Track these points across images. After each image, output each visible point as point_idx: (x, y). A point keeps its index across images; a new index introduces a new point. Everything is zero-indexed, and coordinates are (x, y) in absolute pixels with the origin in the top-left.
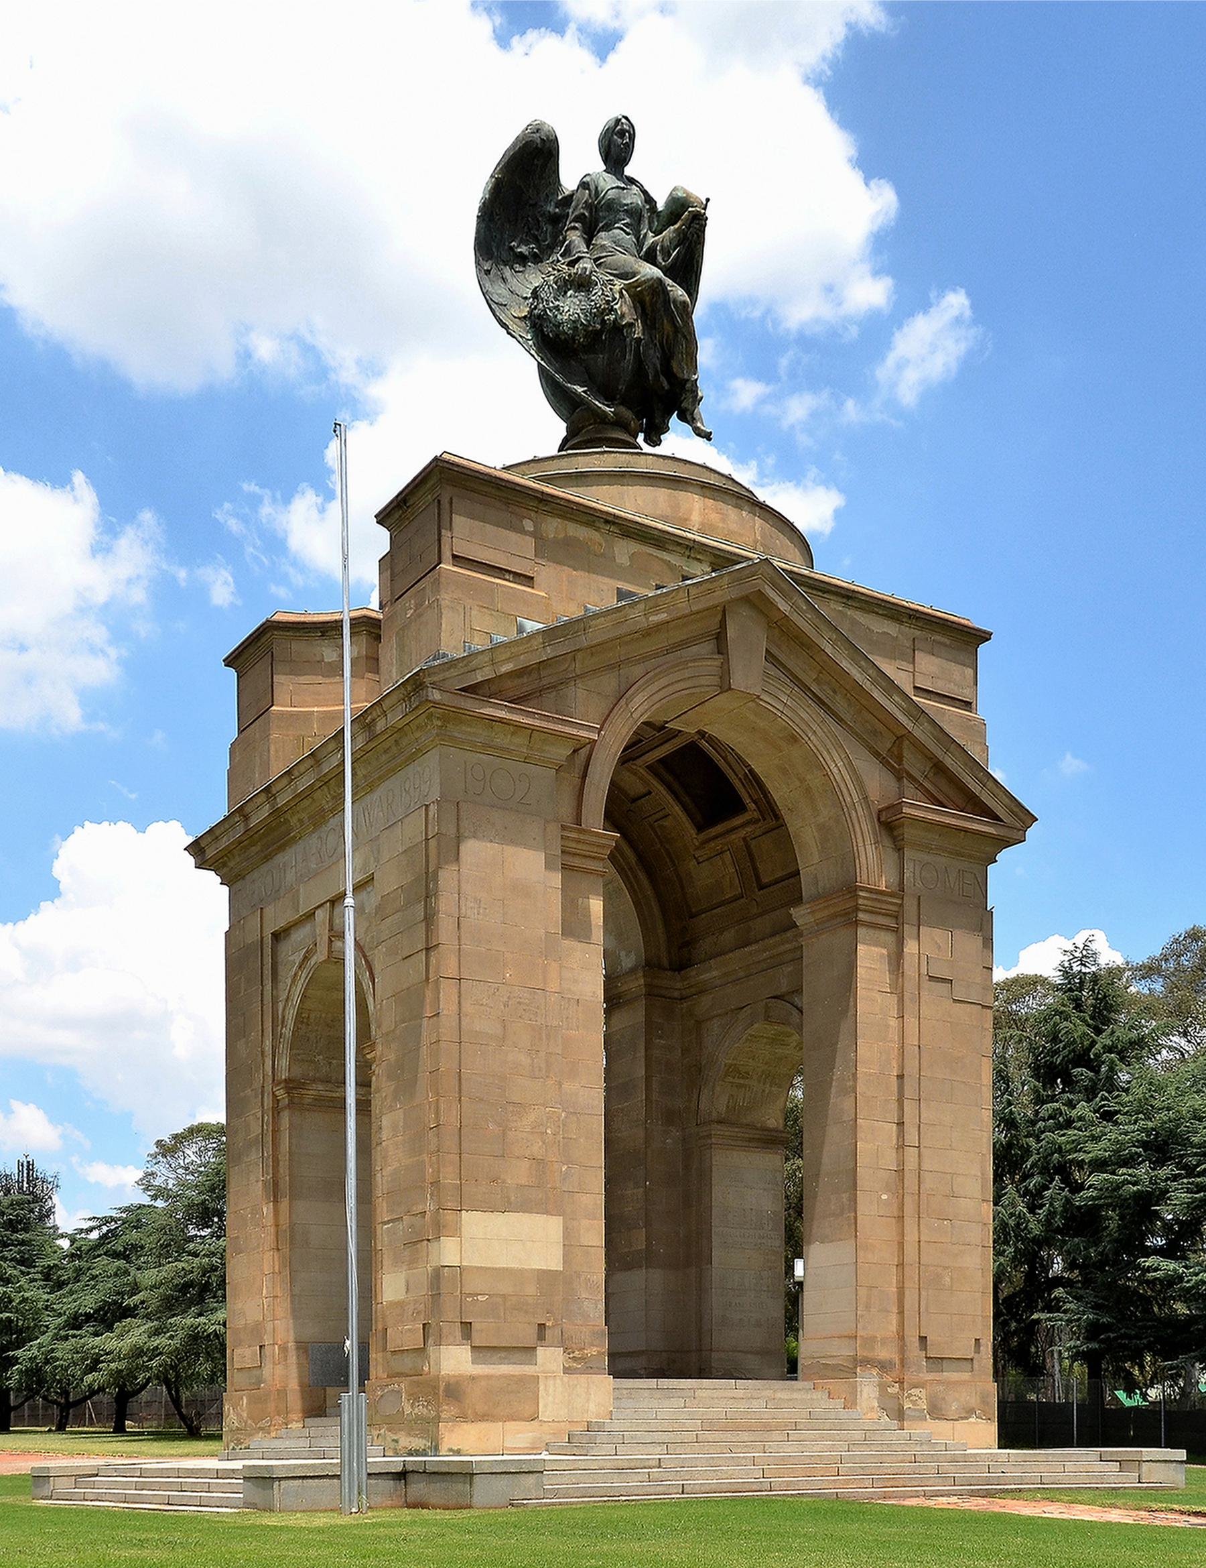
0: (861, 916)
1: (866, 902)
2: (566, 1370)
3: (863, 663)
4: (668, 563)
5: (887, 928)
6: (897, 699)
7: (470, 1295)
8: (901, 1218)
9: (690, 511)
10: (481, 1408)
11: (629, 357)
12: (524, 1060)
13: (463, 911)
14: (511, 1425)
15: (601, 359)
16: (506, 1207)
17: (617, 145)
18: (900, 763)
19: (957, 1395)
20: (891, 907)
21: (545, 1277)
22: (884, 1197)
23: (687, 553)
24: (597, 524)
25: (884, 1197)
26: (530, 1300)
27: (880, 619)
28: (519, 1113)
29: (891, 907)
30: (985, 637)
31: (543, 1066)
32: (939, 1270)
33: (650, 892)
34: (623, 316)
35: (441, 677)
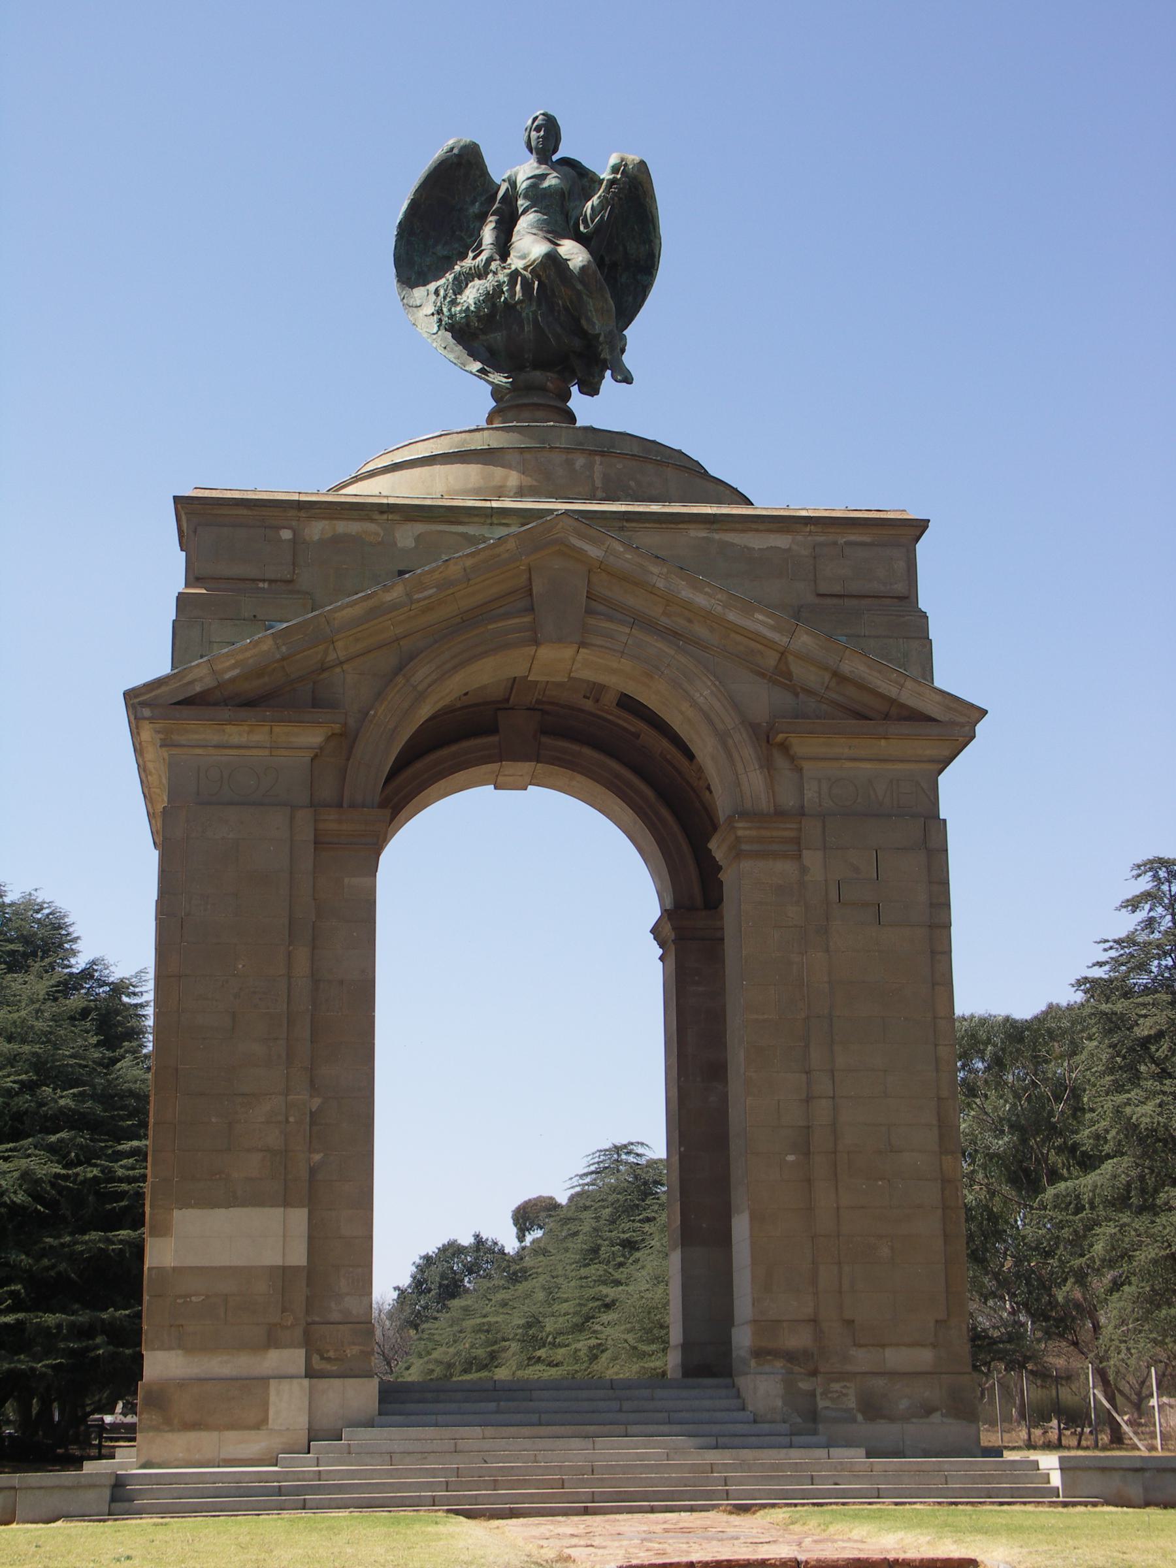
0: (744, 847)
1: (747, 833)
2: (310, 1374)
3: (707, 589)
6: (761, 617)
7: (179, 1297)
14: (231, 1435)
16: (232, 1200)
17: (547, 135)
18: (790, 679)
21: (285, 1273)
22: (791, 1158)
23: (489, 521)
25: (791, 1158)
30: (921, 526)
33: (676, 828)
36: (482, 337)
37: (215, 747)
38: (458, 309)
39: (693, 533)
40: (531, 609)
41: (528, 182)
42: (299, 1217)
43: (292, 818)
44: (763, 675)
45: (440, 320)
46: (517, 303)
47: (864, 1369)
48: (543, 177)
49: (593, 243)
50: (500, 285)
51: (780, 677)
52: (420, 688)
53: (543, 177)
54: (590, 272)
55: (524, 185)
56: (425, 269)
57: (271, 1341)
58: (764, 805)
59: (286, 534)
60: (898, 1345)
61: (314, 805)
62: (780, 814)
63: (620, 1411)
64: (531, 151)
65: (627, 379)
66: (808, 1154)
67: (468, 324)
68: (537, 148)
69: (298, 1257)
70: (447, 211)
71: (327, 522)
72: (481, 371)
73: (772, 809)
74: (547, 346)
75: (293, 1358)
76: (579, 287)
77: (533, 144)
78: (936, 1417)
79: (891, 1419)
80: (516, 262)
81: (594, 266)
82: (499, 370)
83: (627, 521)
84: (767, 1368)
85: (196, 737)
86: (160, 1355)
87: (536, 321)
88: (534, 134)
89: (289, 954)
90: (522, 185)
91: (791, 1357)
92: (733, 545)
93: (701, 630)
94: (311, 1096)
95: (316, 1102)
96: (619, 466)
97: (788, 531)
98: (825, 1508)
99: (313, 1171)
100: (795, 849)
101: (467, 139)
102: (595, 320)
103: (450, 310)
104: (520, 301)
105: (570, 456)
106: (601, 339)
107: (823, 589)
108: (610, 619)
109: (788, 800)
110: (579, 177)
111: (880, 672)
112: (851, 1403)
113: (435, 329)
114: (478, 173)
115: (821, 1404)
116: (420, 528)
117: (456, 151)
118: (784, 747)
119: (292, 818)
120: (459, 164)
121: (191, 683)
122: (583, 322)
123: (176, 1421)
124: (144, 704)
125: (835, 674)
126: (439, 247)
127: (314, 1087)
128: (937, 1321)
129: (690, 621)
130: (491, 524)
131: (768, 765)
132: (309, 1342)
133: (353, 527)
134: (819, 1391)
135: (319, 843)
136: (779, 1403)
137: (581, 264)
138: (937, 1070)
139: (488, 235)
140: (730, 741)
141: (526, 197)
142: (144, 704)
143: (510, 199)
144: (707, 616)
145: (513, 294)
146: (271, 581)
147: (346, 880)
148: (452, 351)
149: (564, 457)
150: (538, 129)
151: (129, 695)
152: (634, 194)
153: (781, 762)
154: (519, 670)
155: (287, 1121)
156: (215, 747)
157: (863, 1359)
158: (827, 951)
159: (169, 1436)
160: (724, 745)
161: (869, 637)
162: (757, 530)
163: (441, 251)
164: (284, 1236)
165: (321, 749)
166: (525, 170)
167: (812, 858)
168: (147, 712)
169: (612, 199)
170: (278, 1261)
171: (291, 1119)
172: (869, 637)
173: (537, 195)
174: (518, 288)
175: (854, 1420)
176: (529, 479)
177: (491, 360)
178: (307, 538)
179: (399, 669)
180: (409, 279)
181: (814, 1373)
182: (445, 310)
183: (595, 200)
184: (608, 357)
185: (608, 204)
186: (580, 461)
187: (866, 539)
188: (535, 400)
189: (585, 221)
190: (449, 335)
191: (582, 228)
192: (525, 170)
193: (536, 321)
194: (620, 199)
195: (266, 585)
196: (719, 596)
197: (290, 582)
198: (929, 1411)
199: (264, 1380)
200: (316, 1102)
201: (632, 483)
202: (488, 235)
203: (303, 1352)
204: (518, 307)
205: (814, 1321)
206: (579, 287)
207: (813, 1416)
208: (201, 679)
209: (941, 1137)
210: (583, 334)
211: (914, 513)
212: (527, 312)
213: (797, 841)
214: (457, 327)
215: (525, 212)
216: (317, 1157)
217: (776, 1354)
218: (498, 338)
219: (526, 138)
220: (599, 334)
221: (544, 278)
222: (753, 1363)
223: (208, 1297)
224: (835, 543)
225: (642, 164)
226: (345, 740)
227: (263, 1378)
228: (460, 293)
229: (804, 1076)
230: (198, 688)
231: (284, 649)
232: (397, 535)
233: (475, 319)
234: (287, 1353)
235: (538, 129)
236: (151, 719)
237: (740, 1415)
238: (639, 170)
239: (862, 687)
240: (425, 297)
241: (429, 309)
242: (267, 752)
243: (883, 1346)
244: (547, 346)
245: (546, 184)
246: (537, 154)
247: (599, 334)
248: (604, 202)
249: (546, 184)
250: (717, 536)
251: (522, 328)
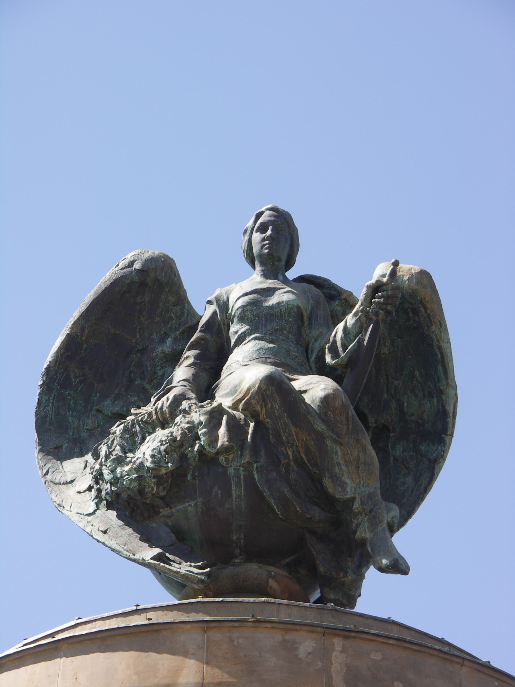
17: (278, 242)
36: (165, 511)
38: (127, 468)
41: (246, 299)
45: (98, 495)
46: (218, 453)
48: (269, 292)
49: (345, 381)
50: (192, 428)
53: (269, 292)
54: (338, 404)
55: (240, 303)
56: (85, 435)
64: (252, 262)
65: (398, 567)
68: (260, 255)
72: (158, 558)
76: (320, 426)
77: (256, 249)
80: (224, 398)
81: (344, 397)
82: (187, 557)
87: (249, 479)
88: (257, 237)
90: (236, 304)
96: (377, 656)
98: (223, 624)
101: (154, 250)
102: (346, 479)
103: (113, 471)
104: (226, 450)
105: (289, 637)
106: (357, 506)
110: (326, 296)
113: (92, 507)
114: (172, 299)
117: (137, 266)
120: (143, 284)
122: (327, 482)
126: (107, 402)
137: (322, 394)
141: (242, 319)
143: (218, 326)
145: (213, 438)
148: (117, 536)
149: (278, 636)
150: (263, 229)
152: (408, 325)
163: (108, 406)
166: (242, 285)
169: (377, 314)
173: (258, 315)
174: (222, 431)
176: (217, 671)
177: (176, 542)
180: (58, 448)
182: (106, 472)
183: (350, 320)
184: (368, 535)
185: (369, 320)
186: (307, 645)
189: (334, 350)
190: (112, 514)
191: (328, 359)
192: (242, 285)
194: (388, 313)
204: (222, 459)
206: (320, 426)
210: (328, 501)
212: (235, 467)
214: (124, 495)
215: (240, 341)
218: (188, 511)
219: (244, 245)
220: (353, 500)
221: (263, 417)
225: (424, 278)
228: (133, 451)
233: (152, 482)
235: (263, 229)
238: (418, 283)
240: (77, 469)
241: (88, 480)
245: (273, 301)
246: (262, 264)
247: (353, 500)
248: (361, 325)
249: (273, 301)
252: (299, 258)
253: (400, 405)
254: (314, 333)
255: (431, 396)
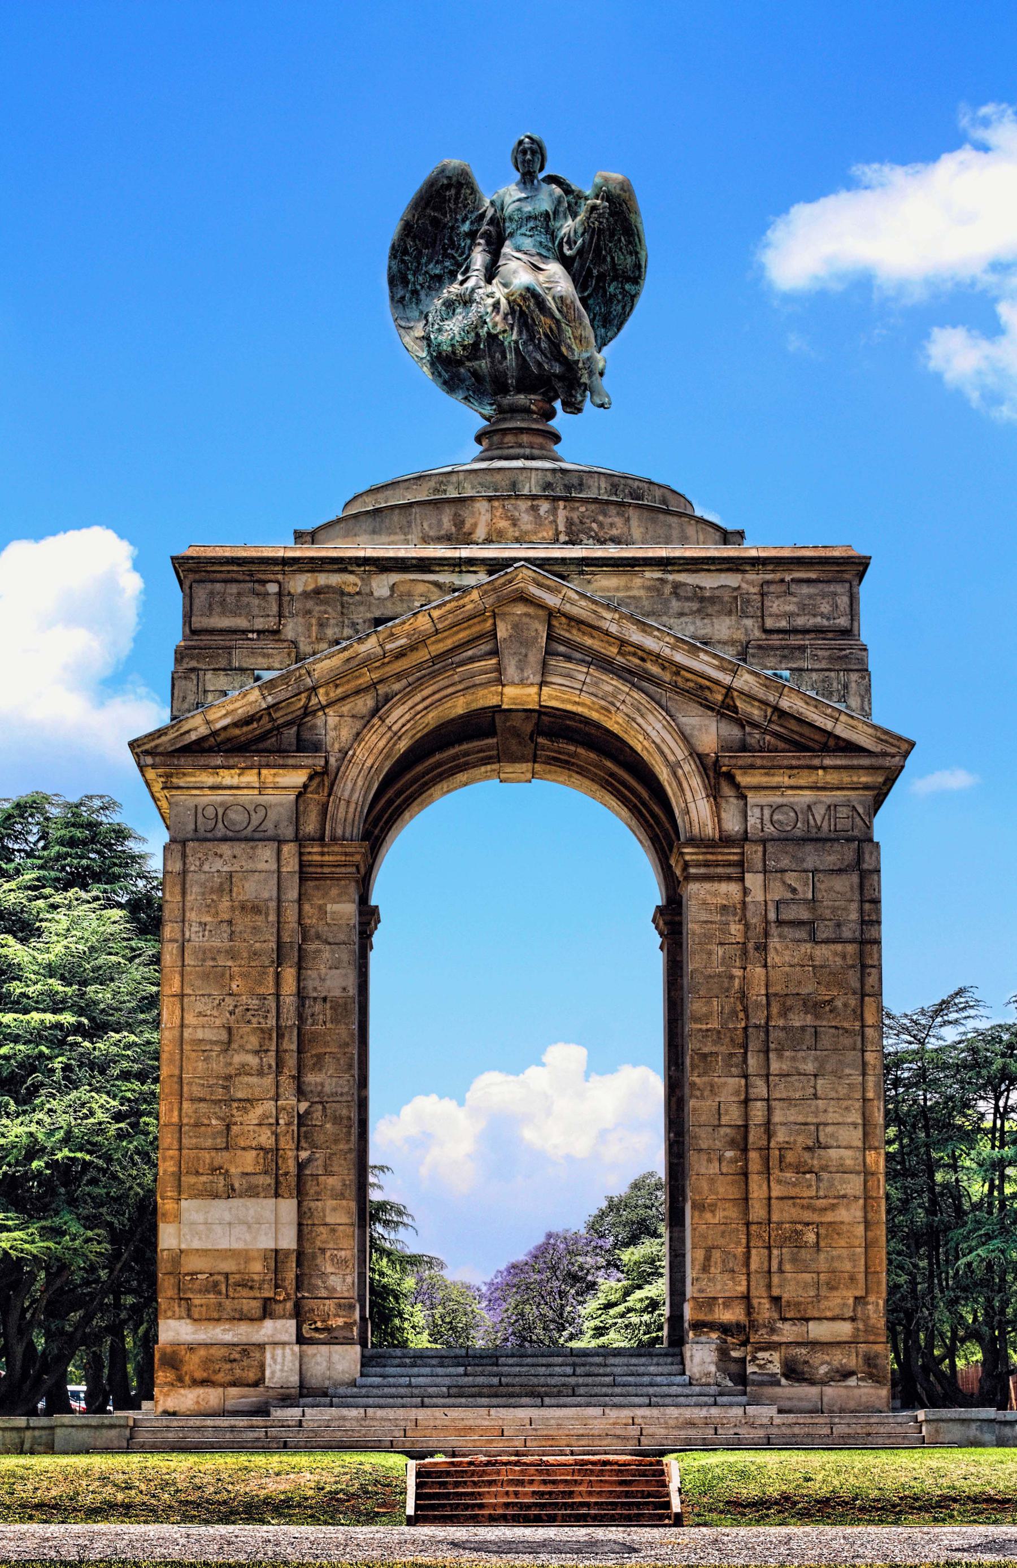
1: (694, 857)
3: (656, 633)
4: (436, 584)
5: (729, 878)
8: (745, 1174)
9: (475, 525)
10: (199, 1375)
11: (510, 356)
12: (253, 1060)
13: (187, 936)
15: (484, 365)
17: (529, 160)
18: (737, 713)
19: (827, 1358)
20: (731, 857)
24: (350, 568)
26: (256, 1277)
27: (714, 574)
28: (245, 1108)
29: (731, 857)
30: (860, 566)
31: (274, 1064)
32: (799, 1227)
34: (495, 325)
35: (153, 744)
36: (468, 364)
37: (211, 788)
39: (648, 575)
40: (495, 652)
42: (288, 1207)
43: (279, 852)
44: (712, 709)
47: (790, 1340)
51: (725, 709)
52: (395, 728)
57: (267, 1311)
58: (710, 830)
59: (273, 588)
60: (819, 1319)
61: (299, 840)
62: (726, 840)
63: (574, 1375)
66: (745, 1150)
67: (454, 353)
69: (288, 1241)
70: (440, 228)
71: (309, 575)
73: (717, 836)
74: (521, 381)
75: (284, 1328)
78: (852, 1381)
79: (812, 1382)
83: (587, 565)
84: (703, 1339)
85: (193, 779)
86: (172, 1323)
87: (517, 349)
89: (278, 975)
91: (725, 1329)
92: (685, 584)
93: (654, 669)
94: (299, 1101)
95: (303, 1106)
97: (738, 570)
99: (301, 1166)
100: (740, 870)
102: (574, 346)
105: (535, 503)
106: (580, 365)
107: (769, 623)
108: (569, 659)
109: (732, 825)
111: (816, 707)
112: (776, 1368)
115: (750, 1369)
116: (395, 577)
118: (730, 778)
119: (279, 852)
121: (188, 732)
122: (564, 349)
123: (187, 1378)
124: (147, 753)
125: (776, 709)
126: (431, 266)
127: (301, 1093)
128: (856, 1298)
129: (643, 660)
130: (461, 572)
131: (714, 794)
132: (299, 1314)
133: (334, 579)
134: (749, 1358)
135: (304, 876)
136: (713, 1369)
138: (864, 1074)
139: (479, 258)
140: (680, 772)
142: (147, 753)
144: (657, 657)
146: (259, 632)
147: (329, 906)
149: (529, 503)
151: (133, 745)
153: (727, 790)
154: (494, 701)
155: (278, 1124)
156: (211, 788)
157: (788, 1332)
158: (765, 966)
159: (182, 1391)
160: (675, 774)
161: (812, 670)
162: (709, 570)
164: (276, 1223)
165: (305, 786)
167: (754, 881)
168: (149, 760)
170: (272, 1246)
171: (281, 1122)
172: (812, 670)
175: (778, 1384)
178: (292, 591)
179: (375, 712)
181: (745, 1343)
186: (545, 506)
187: (813, 576)
188: (519, 424)
193: (517, 349)
195: (255, 636)
196: (667, 639)
197: (277, 632)
198: (846, 1374)
199: (261, 1347)
200: (303, 1106)
201: (594, 526)
202: (479, 258)
203: (293, 1322)
205: (747, 1298)
207: (741, 1379)
208: (195, 729)
209: (865, 1134)
211: (859, 550)
213: (740, 864)
216: (304, 1155)
217: (712, 1326)
222: (691, 1334)
223: (211, 1274)
224: (782, 581)
226: (324, 778)
227: (259, 1345)
229: (743, 1081)
230: (193, 736)
231: (269, 699)
232: (374, 585)
234: (280, 1323)
236: (154, 766)
237: (678, 1379)
239: (800, 721)
242: (256, 792)
243: (807, 1320)
244: (521, 381)
250: (670, 577)
251: (504, 357)
252: (547, 165)
253: (613, 258)
254: (558, 224)
255: (631, 254)
